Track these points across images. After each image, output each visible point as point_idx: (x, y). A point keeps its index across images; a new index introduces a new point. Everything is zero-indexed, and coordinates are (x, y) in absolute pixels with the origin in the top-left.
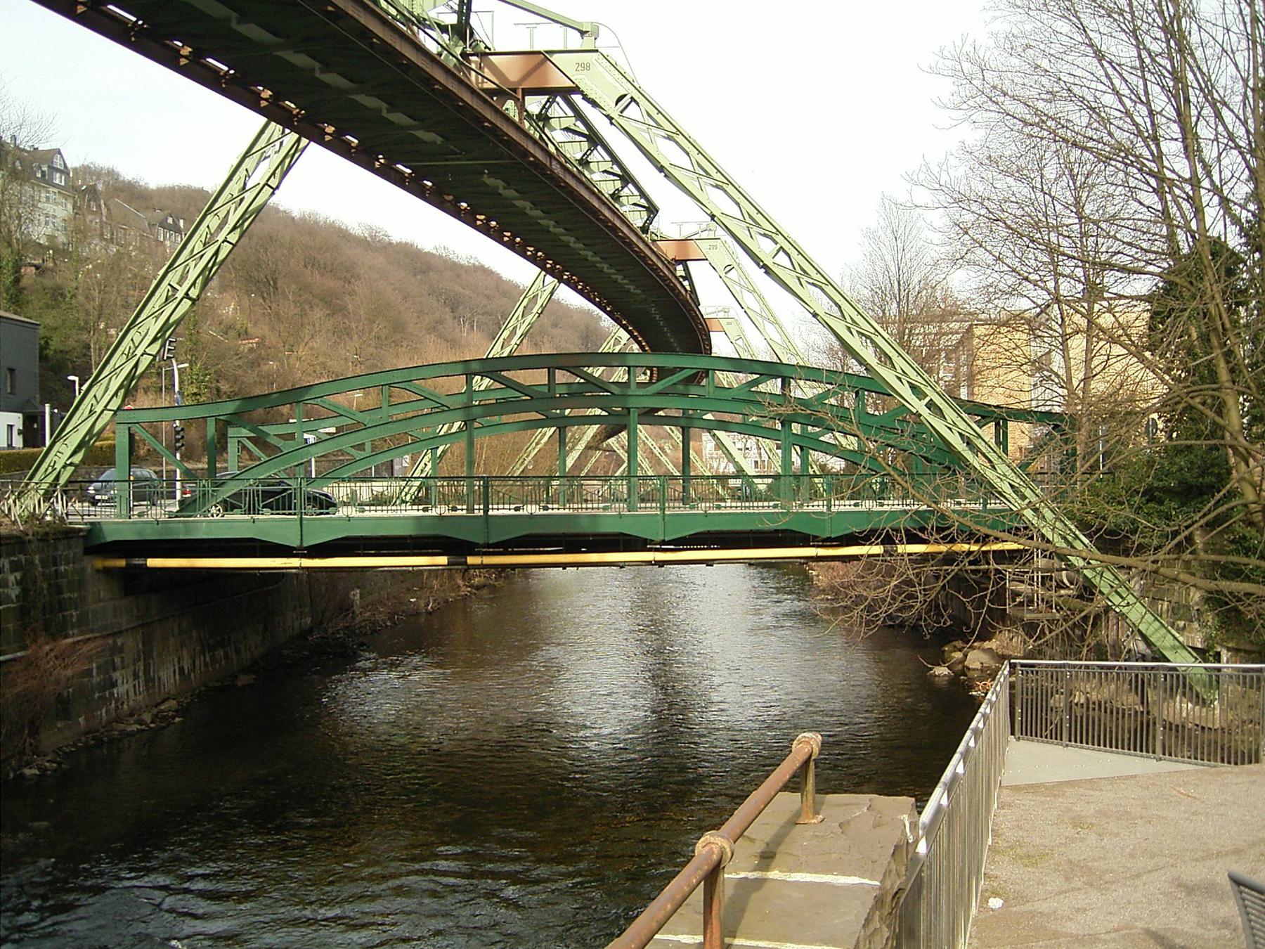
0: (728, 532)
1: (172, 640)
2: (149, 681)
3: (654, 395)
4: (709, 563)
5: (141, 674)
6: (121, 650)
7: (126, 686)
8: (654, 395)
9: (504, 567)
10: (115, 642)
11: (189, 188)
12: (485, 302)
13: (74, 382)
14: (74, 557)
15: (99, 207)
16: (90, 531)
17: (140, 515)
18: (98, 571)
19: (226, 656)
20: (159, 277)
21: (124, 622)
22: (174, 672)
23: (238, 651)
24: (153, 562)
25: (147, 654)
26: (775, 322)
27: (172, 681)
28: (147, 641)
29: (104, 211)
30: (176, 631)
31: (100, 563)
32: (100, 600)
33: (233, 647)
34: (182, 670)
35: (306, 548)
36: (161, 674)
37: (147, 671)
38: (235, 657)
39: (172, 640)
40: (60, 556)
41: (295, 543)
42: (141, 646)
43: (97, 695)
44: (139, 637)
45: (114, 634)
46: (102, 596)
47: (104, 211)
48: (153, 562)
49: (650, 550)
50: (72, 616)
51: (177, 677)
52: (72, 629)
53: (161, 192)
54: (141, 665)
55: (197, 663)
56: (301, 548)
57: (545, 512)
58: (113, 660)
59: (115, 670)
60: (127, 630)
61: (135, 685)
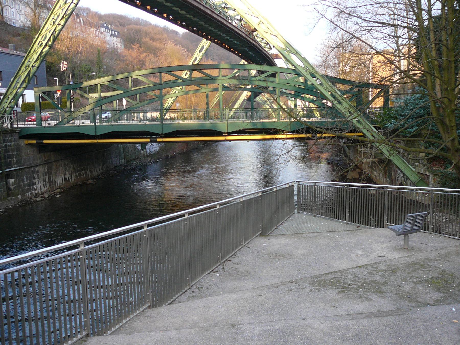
0: (122, 132)
1: (60, 168)
2: (51, 183)
3: (228, 79)
4: (248, 140)
5: (47, 180)
6: (37, 172)
7: (40, 185)
8: (228, 79)
9: (206, 142)
10: (34, 169)
11: (115, 14)
12: (217, 51)
13: (56, 80)
14: (14, 140)
15: (80, 20)
16: (20, 131)
17: (72, 123)
18: (26, 145)
19: (86, 173)
20: (36, 38)
21: (39, 162)
22: (62, 179)
23: (91, 172)
24: (45, 141)
25: (49, 173)
26: (297, 53)
27: (61, 182)
28: (50, 169)
29: (82, 22)
30: (63, 165)
31: (26, 142)
32: (28, 155)
33: (89, 170)
34: (65, 179)
35: (99, 136)
36: (56, 180)
37: (49, 179)
38: (90, 174)
39: (60, 168)
40: (8, 140)
41: (93, 134)
42: (46, 171)
43: (26, 188)
44: (46, 168)
45: (34, 166)
46: (29, 153)
47: (82, 22)
48: (45, 141)
49: (224, 136)
50: (14, 160)
51: (64, 181)
52: (14, 165)
53: (105, 16)
54: (47, 177)
55: (73, 176)
56: (162, 134)
57: (83, 125)
58: (34, 176)
59: (34, 179)
60: (40, 165)
61: (44, 184)
